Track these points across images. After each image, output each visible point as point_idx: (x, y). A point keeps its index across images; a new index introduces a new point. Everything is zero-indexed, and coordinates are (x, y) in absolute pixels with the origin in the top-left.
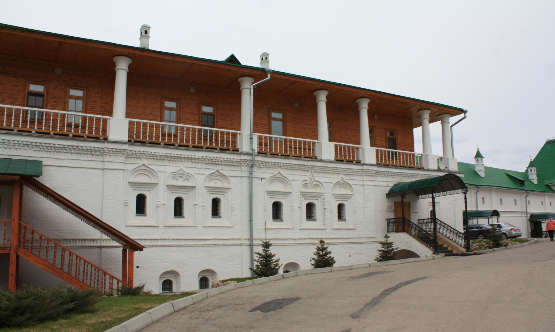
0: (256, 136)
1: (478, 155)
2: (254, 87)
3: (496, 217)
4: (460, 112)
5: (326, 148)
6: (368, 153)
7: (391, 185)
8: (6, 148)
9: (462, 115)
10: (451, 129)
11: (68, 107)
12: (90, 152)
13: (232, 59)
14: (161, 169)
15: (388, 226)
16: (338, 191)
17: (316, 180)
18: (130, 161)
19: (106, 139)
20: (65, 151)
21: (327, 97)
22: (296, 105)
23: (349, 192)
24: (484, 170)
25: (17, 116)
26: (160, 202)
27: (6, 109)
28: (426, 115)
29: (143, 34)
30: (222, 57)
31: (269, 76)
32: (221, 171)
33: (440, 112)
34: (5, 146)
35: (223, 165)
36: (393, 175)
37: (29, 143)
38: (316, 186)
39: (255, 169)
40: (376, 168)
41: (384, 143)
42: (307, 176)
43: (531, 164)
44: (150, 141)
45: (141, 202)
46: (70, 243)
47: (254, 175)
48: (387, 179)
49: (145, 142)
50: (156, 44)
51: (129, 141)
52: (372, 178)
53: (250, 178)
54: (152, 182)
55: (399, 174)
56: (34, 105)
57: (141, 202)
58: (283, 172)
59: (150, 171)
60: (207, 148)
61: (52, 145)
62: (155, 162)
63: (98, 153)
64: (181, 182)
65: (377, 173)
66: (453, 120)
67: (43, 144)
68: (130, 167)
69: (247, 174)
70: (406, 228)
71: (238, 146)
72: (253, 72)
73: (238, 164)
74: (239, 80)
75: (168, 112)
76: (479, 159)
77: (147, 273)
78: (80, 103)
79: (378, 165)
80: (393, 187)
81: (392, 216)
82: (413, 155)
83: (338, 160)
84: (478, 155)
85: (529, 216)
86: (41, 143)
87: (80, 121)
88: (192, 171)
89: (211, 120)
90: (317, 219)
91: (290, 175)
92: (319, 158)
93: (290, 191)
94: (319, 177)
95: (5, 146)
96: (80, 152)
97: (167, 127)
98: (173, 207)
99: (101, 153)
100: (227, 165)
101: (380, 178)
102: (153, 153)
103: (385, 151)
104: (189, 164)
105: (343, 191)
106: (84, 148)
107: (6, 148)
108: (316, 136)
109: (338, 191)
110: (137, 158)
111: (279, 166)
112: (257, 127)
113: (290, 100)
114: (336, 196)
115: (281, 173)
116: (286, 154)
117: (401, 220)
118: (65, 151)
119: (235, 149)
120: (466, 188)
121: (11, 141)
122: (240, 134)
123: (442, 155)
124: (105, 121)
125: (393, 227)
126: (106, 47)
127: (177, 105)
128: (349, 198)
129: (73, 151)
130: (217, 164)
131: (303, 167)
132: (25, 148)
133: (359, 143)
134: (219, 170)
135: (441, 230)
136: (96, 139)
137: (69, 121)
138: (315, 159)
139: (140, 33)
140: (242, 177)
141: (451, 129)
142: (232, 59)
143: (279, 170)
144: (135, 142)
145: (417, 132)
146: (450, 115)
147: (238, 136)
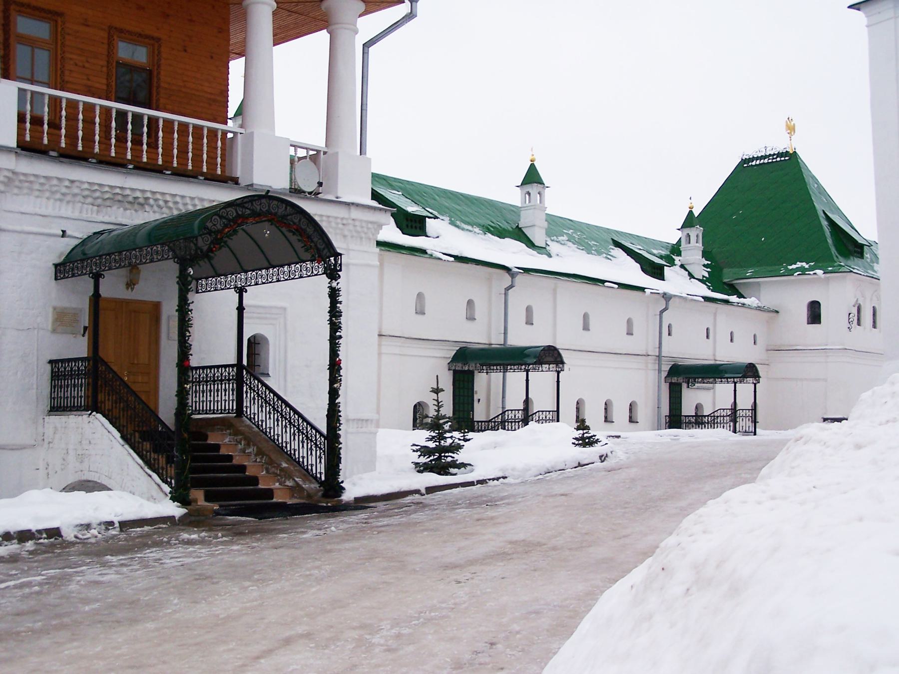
1: (532, 177)
3: (751, 380)
7: (79, 232)
10: (365, 53)
11: (11, 71)
15: (53, 387)
24: (546, 224)
27: (176, 124)
41: (100, 83)
43: (690, 221)
48: (67, 210)
56: (29, 76)
70: (100, 397)
75: (28, 49)
76: (534, 189)
78: (43, 57)
80: (84, 242)
81: (79, 347)
82: (225, 133)
84: (532, 177)
85: (666, 368)
87: (46, 109)
89: (140, 87)
103: (106, 111)
117: (233, 372)
123: (319, 142)
125: (80, 393)
127: (55, 33)
137: (37, 113)
141: (365, 53)
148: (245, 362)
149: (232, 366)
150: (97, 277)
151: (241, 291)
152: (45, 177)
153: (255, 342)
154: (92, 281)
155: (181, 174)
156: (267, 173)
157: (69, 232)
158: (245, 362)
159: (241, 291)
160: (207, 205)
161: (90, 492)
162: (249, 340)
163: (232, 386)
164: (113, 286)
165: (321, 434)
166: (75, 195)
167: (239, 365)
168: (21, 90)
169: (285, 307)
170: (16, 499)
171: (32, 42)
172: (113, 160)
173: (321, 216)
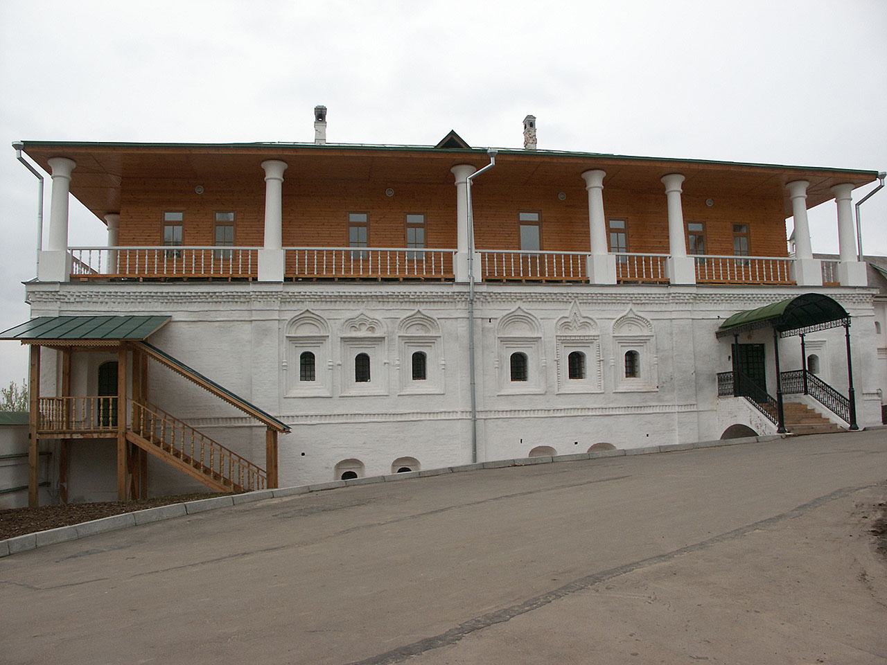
0: (477, 258)
2: (473, 179)
4: (871, 177)
5: (602, 263)
6: (682, 265)
8: (127, 303)
9: (877, 183)
10: (857, 209)
12: (233, 298)
13: (452, 141)
14: (333, 315)
16: (626, 331)
17: (585, 316)
18: (288, 307)
19: (255, 279)
20: (199, 300)
21: (605, 182)
22: (562, 197)
23: (646, 332)
25: (198, 258)
26: (334, 360)
27: (546, 256)
28: (800, 193)
29: (528, 127)
30: (431, 138)
31: (492, 160)
32: (423, 312)
33: (829, 183)
34: (125, 300)
35: (427, 302)
36: (729, 299)
37: (152, 294)
38: (585, 325)
39: (478, 305)
40: (694, 290)
42: (566, 311)
44: (318, 276)
45: (308, 362)
46: (511, 415)
47: (477, 314)
48: (719, 307)
49: (561, 281)
50: (340, 133)
51: (618, 282)
52: (689, 307)
53: (471, 319)
54: (322, 334)
55: (740, 298)
57: (308, 362)
58: (525, 306)
59: (318, 320)
60: (547, 281)
61: (181, 294)
62: (324, 306)
63: (242, 300)
64: (363, 333)
65: (696, 297)
66: (858, 193)
67: (170, 294)
68: (289, 316)
69: (466, 315)
71: (589, 275)
72: (66, 150)
73: (451, 299)
74: (583, 176)
77: (312, 457)
79: (700, 284)
83: (487, 280)
86: (168, 293)
88: (378, 316)
90: (628, 378)
91: (536, 310)
92: (672, 283)
93: (539, 336)
94: (586, 311)
95: (125, 300)
96: (220, 300)
97: (231, 251)
98: (371, 364)
99: (247, 298)
100: (434, 302)
101: (703, 306)
102: (319, 294)
104: (374, 305)
105: (635, 331)
106: (223, 294)
107: (127, 303)
108: (667, 249)
109: (626, 331)
110: (298, 302)
111: (358, 298)
112: (480, 240)
113: (535, 194)
114: (620, 340)
115: (522, 308)
116: (534, 278)
117: (802, 374)
118: (199, 300)
119: (448, 276)
120: (847, 316)
121: (131, 294)
122: (670, 257)
124: (255, 253)
125: (730, 387)
126: (204, 152)
128: (645, 341)
129: (209, 300)
130: (417, 302)
131: (561, 298)
132: (150, 300)
133: (588, 249)
134: (420, 310)
135: (813, 390)
136: (576, 282)
138: (667, 283)
139: (523, 126)
140: (251, 321)
142: (452, 141)
143: (519, 303)
144: (548, 281)
145: (790, 222)
146: (853, 186)
147: (838, 264)
148: (807, 369)
149: (801, 371)
150: (736, 336)
151: (802, 336)
152: (207, 293)
153: (812, 359)
154: (734, 338)
155: (774, 286)
156: (810, 278)
157: (721, 317)
158: (807, 369)
159: (802, 336)
160: (796, 296)
161: (355, 459)
162: (808, 358)
163: (802, 380)
164: (743, 340)
165: (847, 400)
166: (722, 300)
167: (804, 370)
168: (822, 262)
169: (825, 340)
170: (355, 458)
171: (359, 225)
172: (496, 278)
173: (831, 295)
